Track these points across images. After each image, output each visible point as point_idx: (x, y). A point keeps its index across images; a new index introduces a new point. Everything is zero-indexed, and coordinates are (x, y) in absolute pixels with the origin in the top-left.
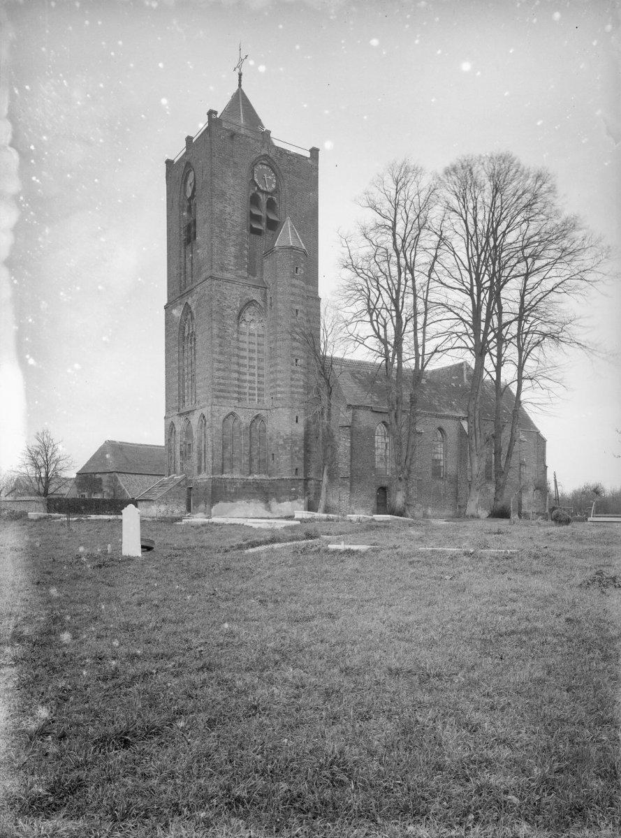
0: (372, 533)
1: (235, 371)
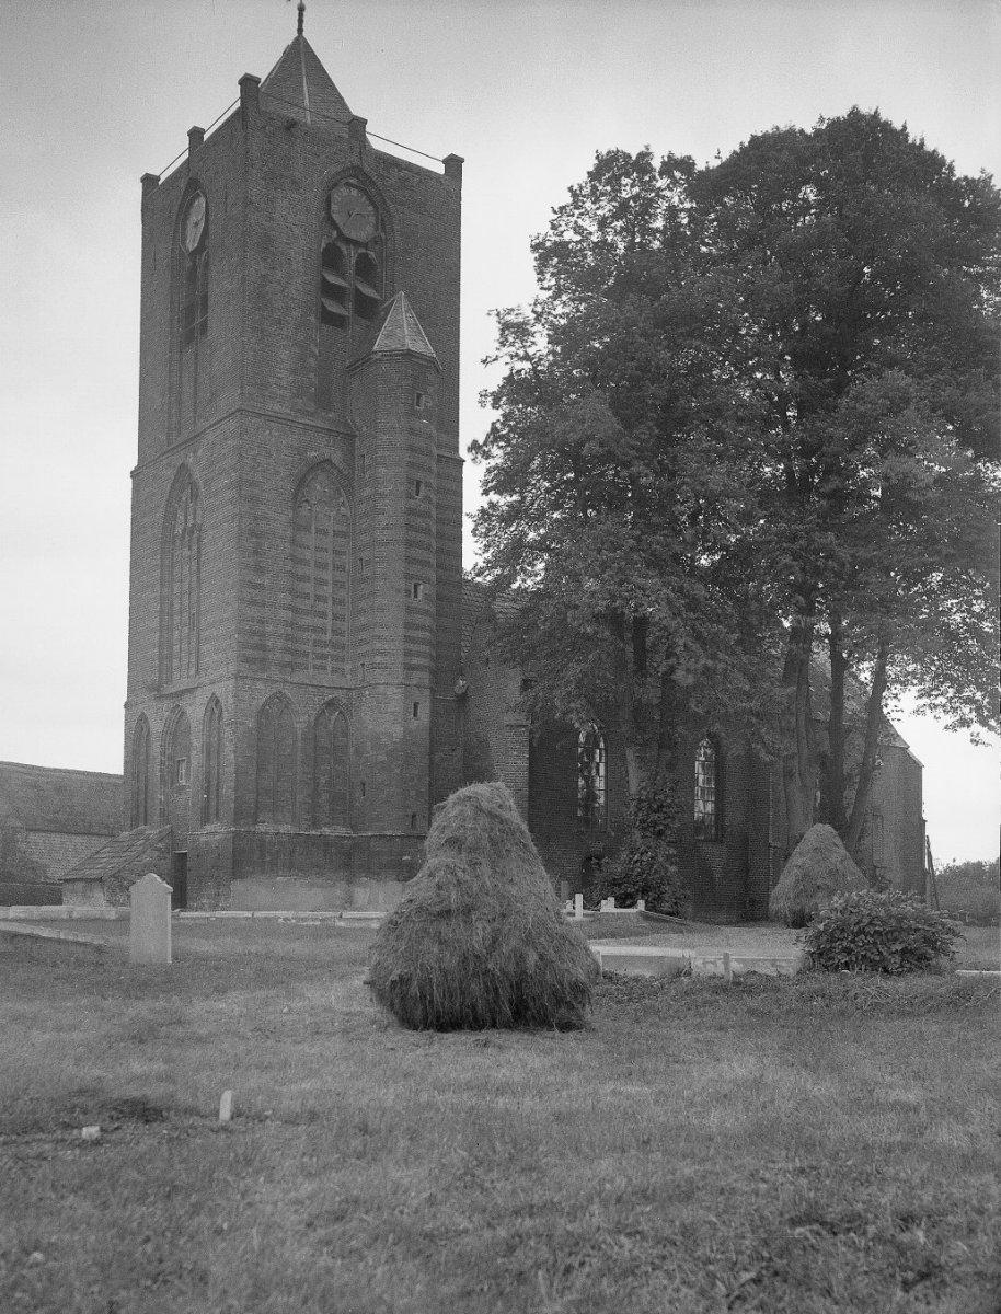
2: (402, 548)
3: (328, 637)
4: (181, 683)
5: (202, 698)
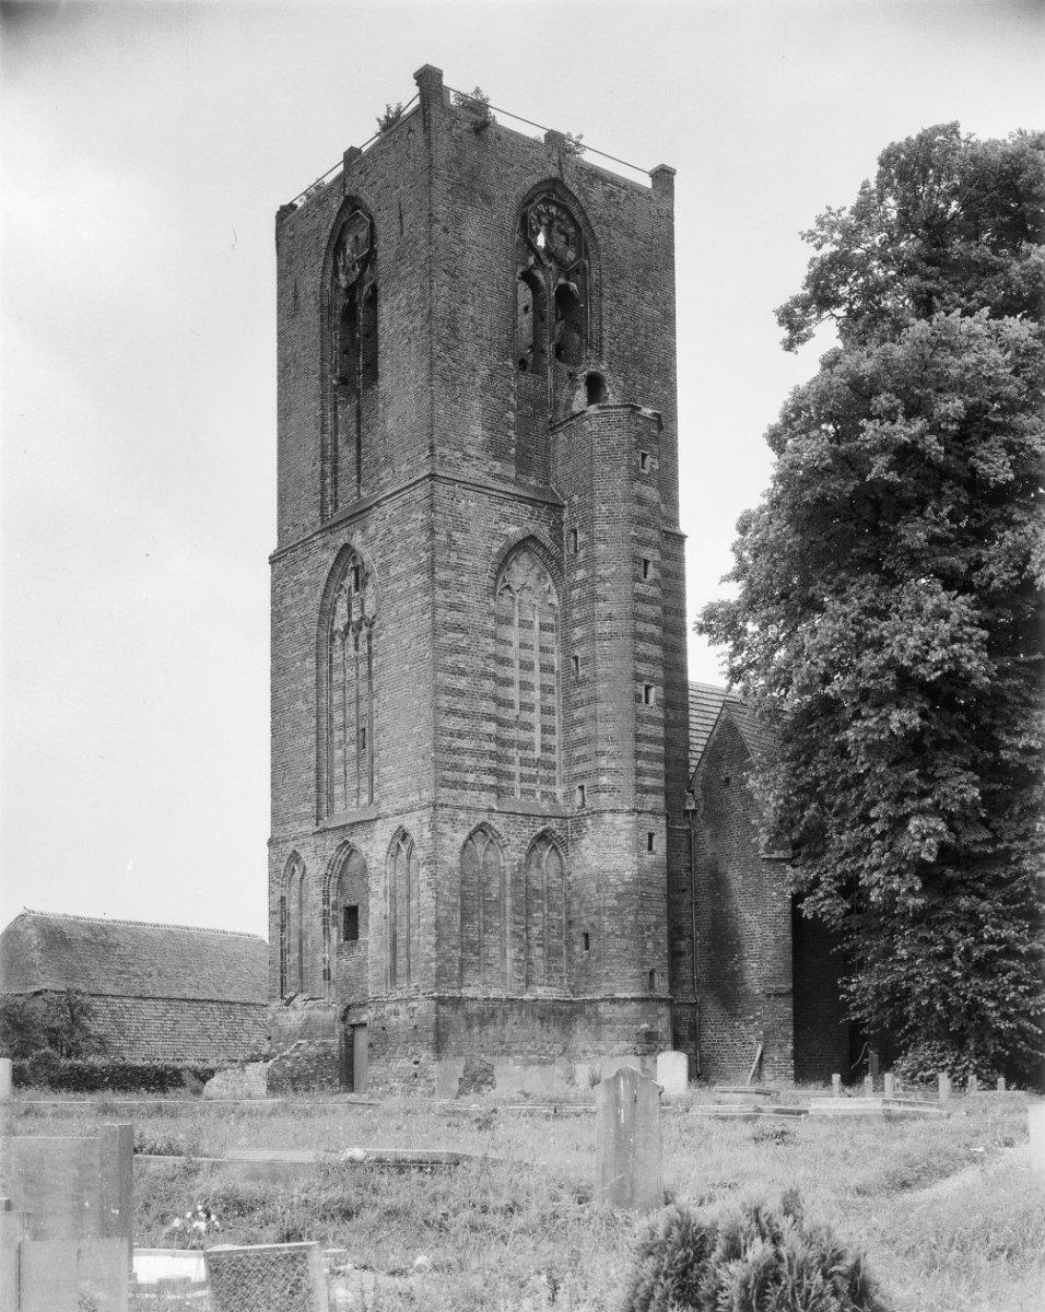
0: (379, 741)
1: (490, 718)
2: (629, 641)
3: (537, 754)
4: (344, 811)
5: (383, 833)
